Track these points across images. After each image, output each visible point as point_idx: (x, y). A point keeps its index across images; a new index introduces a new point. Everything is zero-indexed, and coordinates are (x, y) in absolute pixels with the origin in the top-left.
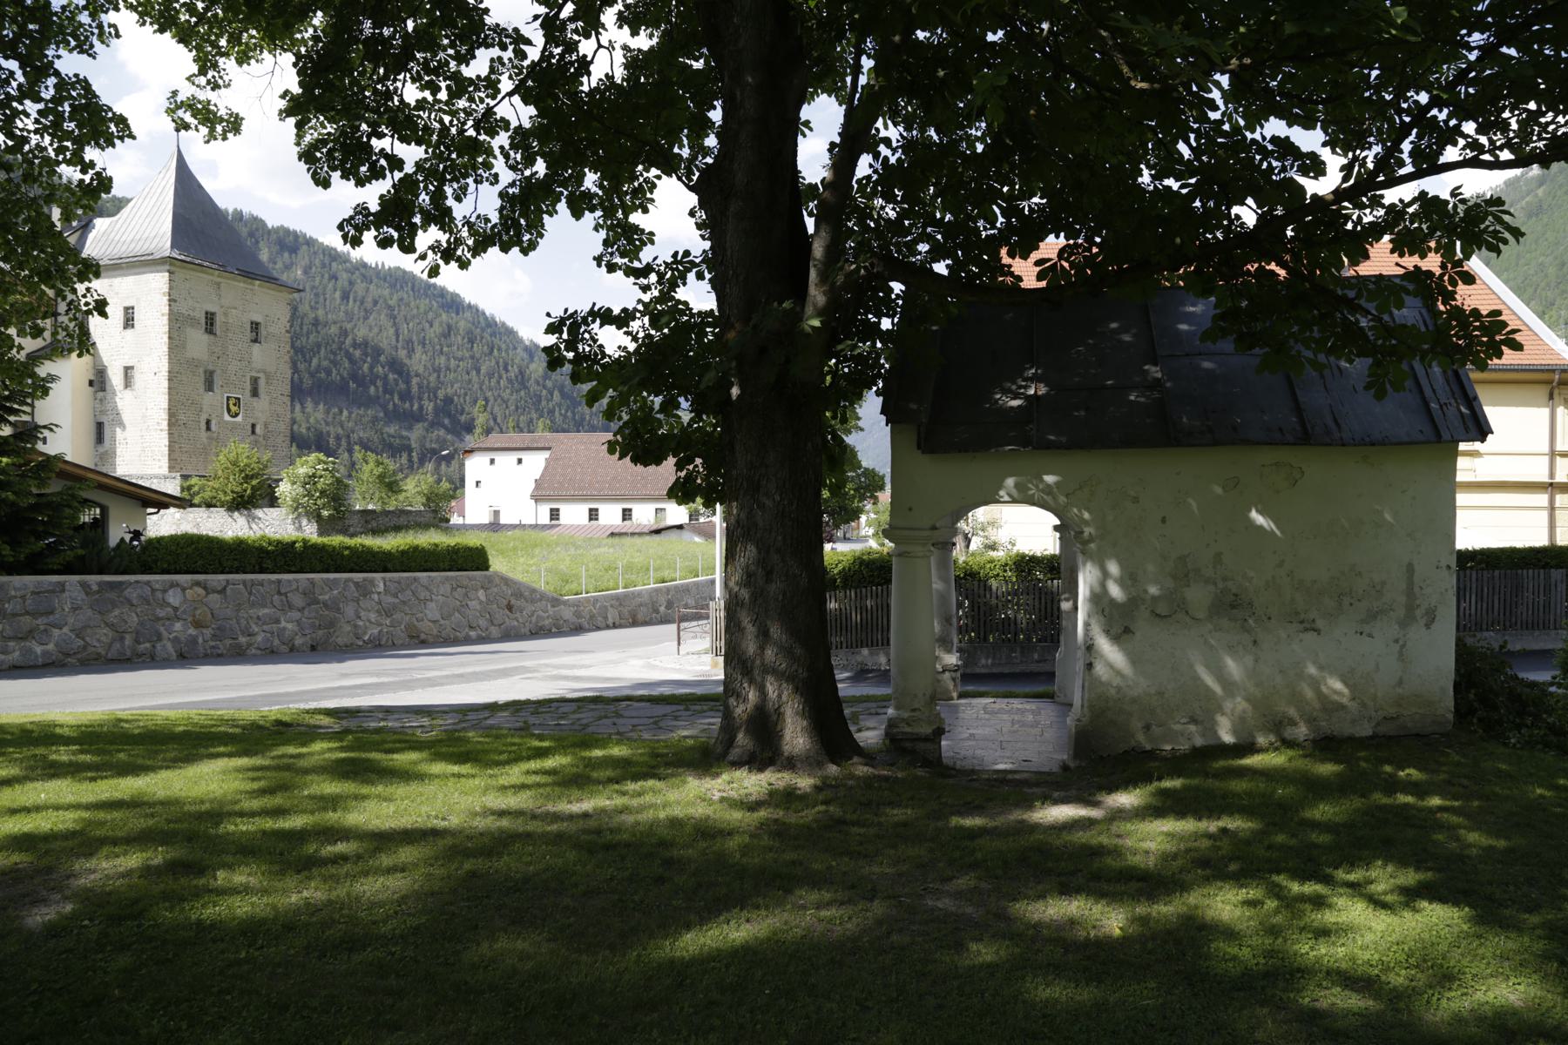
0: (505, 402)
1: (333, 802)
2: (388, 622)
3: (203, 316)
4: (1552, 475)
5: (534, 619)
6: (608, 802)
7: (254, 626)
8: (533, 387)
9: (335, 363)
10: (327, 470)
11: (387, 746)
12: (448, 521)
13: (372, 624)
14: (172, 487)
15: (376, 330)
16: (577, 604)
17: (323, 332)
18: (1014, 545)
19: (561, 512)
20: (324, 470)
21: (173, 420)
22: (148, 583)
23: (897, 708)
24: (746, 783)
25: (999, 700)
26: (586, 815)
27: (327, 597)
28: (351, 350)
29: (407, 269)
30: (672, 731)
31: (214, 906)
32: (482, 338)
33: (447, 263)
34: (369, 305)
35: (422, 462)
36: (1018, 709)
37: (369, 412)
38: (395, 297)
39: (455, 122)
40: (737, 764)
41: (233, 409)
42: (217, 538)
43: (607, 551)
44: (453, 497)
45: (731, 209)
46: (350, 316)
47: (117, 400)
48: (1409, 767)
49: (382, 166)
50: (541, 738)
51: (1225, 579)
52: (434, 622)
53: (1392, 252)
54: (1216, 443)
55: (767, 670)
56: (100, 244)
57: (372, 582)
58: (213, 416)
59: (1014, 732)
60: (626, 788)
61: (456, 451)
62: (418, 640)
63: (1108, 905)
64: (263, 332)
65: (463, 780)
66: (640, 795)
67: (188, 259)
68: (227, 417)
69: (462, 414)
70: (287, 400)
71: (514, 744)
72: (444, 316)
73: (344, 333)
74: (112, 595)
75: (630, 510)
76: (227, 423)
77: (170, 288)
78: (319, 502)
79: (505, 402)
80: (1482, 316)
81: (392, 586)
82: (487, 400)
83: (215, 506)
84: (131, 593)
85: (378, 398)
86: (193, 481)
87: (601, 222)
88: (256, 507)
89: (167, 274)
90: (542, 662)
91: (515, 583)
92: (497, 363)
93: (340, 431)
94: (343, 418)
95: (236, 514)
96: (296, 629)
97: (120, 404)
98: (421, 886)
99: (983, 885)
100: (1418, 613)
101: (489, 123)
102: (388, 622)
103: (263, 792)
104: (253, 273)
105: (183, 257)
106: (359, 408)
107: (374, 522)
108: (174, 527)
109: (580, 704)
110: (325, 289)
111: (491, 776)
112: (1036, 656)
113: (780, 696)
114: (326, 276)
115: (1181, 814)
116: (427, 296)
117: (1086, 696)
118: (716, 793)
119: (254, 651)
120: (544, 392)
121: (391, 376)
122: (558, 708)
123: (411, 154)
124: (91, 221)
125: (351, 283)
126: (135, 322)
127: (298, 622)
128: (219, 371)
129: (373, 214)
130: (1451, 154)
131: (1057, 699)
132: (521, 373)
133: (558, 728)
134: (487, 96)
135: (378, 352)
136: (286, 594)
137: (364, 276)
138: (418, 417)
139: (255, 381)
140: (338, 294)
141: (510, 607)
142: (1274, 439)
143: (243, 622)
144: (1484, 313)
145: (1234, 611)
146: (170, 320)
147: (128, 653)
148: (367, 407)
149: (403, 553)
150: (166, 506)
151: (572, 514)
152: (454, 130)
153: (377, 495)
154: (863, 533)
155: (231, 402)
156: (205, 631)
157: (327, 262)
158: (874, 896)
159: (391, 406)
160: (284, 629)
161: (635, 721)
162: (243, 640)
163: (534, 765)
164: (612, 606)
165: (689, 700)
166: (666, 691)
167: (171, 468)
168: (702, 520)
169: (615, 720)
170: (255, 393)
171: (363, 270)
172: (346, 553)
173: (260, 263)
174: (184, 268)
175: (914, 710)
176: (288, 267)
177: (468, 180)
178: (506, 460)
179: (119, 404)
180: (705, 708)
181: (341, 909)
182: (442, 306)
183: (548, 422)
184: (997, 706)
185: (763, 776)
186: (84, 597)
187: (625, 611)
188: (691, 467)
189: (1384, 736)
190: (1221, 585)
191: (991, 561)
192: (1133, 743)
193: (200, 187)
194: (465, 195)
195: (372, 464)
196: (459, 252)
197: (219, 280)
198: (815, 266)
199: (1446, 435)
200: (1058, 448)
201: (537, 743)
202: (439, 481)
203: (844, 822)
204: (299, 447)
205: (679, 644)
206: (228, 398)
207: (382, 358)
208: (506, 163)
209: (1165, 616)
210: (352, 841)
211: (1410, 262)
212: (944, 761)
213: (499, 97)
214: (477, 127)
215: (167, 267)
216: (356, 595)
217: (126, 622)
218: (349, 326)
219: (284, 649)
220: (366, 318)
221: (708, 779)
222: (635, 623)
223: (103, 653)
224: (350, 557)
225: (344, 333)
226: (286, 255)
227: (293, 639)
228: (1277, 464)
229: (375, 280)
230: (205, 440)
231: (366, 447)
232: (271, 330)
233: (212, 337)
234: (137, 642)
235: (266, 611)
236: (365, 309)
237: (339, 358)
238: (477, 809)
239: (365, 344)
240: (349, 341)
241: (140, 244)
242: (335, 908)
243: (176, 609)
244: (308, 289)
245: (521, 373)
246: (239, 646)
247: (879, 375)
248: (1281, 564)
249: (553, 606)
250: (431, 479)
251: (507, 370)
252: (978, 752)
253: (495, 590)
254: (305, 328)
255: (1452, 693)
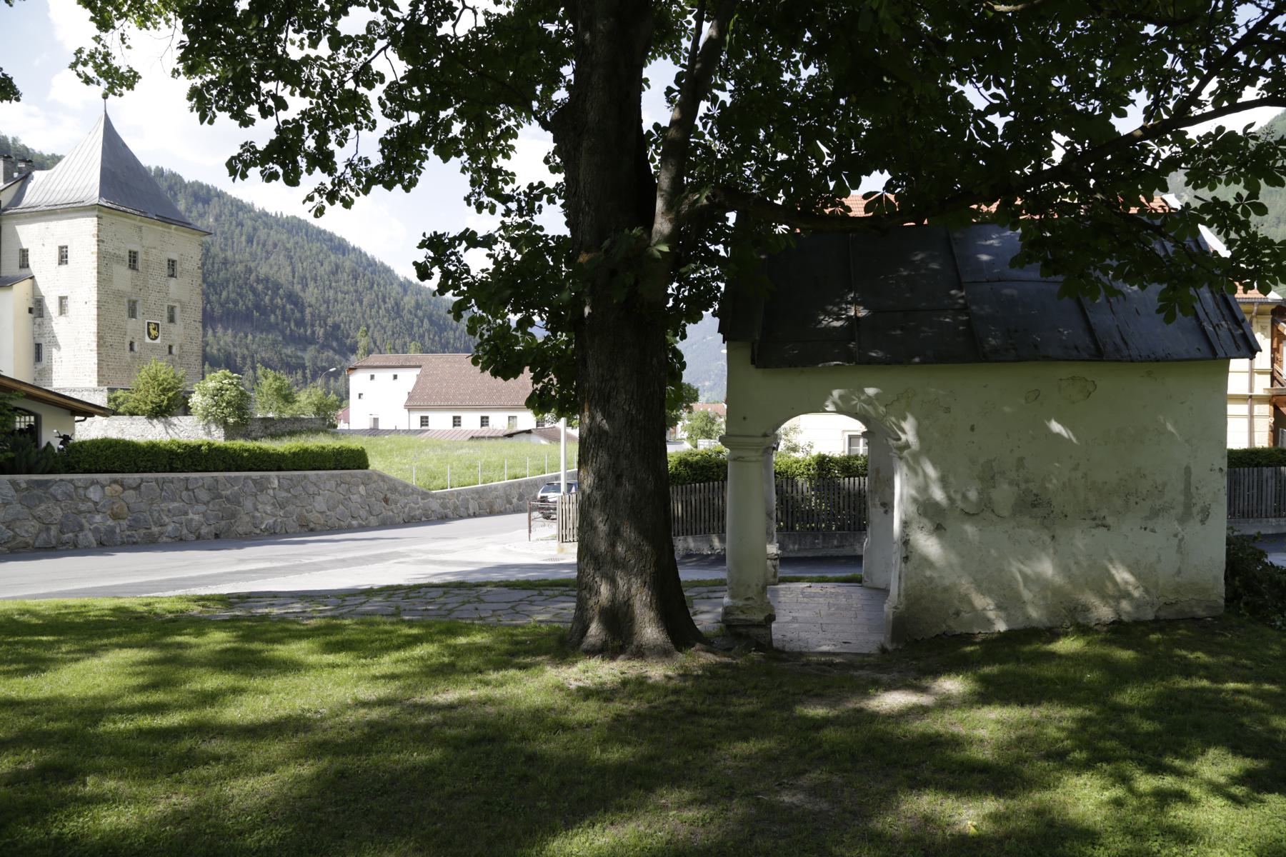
0: (384, 328)
1: (210, 698)
2: (281, 513)
3: (127, 254)
4: (1251, 389)
5: (407, 510)
6: (472, 693)
7: (165, 518)
8: (407, 316)
9: (241, 295)
10: (232, 384)
11: (269, 636)
12: (335, 426)
13: (267, 515)
14: (100, 399)
15: (276, 268)
16: (443, 497)
17: (231, 270)
18: (812, 447)
19: (430, 420)
20: (230, 384)
21: (101, 342)
22: (71, 481)
23: (732, 597)
24: (600, 673)
25: (813, 585)
26: (451, 707)
27: (229, 492)
28: (255, 284)
29: (302, 218)
30: (528, 616)
31: (79, 817)
32: (364, 275)
33: (332, 203)
34: (270, 248)
35: (314, 378)
36: (833, 593)
37: (270, 336)
38: (292, 241)
39: (336, 75)
40: (592, 652)
41: (153, 333)
42: (133, 442)
43: (468, 452)
44: (339, 407)
45: (585, 145)
46: (254, 256)
47: (53, 324)
48: (1200, 650)
49: (270, 107)
50: (411, 624)
51: (1027, 481)
52: (322, 513)
53: (1187, 184)
54: (1019, 359)
55: (618, 564)
56: (38, 194)
57: (268, 479)
58: (136, 339)
59: (831, 615)
60: (489, 678)
61: (342, 368)
62: (307, 529)
63: (957, 798)
64: (178, 268)
65: (337, 670)
66: (502, 685)
67: (114, 206)
68: (148, 340)
69: (347, 338)
70: (199, 326)
71: (386, 632)
72: (333, 257)
73: (249, 270)
74: (39, 492)
75: (487, 418)
76: (147, 344)
77: (99, 231)
78: (225, 411)
79: (384, 328)
80: (1275, 244)
81: (285, 483)
82: (368, 327)
83: (137, 415)
84: (57, 491)
85: (277, 324)
86: (119, 393)
87: (467, 165)
88: (172, 415)
89: (96, 219)
90: (413, 547)
91: (391, 479)
92: (377, 296)
93: (246, 352)
94: (248, 341)
95: (155, 421)
96: (202, 519)
97: (56, 328)
98: (290, 789)
99: (836, 779)
100: (1195, 510)
101: (366, 76)
102: (281, 513)
103: (142, 689)
104: (170, 219)
105: (109, 205)
106: (261, 333)
107: (273, 428)
108: (102, 432)
109: (445, 589)
110: (233, 233)
111: (363, 666)
112: (835, 542)
113: (629, 590)
114: (234, 223)
115: (1005, 701)
116: (318, 240)
117: (903, 585)
118: (573, 682)
119: (165, 539)
120: (416, 320)
121: (288, 307)
122: (426, 593)
123: (297, 105)
124: (30, 173)
125: (255, 229)
126: (69, 259)
127: (204, 514)
128: (140, 302)
129: (259, 152)
130: (1249, 94)
131: (864, 583)
132: (397, 304)
133: (425, 613)
134: (364, 52)
135: (277, 286)
136: (193, 490)
137: (265, 223)
138: (310, 341)
139: (172, 309)
140: (243, 238)
141: (386, 500)
142: (1070, 355)
143: (156, 514)
144: (1277, 241)
145: (1035, 509)
146: (98, 257)
147: (54, 542)
148: (268, 332)
149: (295, 454)
150: (91, 415)
151: (440, 421)
152: (335, 82)
153: (275, 405)
154: (679, 436)
155: (151, 327)
156: (121, 522)
157: (234, 211)
158: (732, 793)
159: (288, 332)
160: (192, 520)
161: (495, 606)
162: (155, 529)
163: (402, 654)
164: (472, 498)
165: (542, 586)
166: (521, 576)
167: (100, 383)
168: (547, 426)
169: (477, 605)
170: (172, 320)
171: (265, 219)
172: (246, 454)
173: (179, 213)
174: (110, 213)
175: (747, 599)
176: (201, 216)
177: (348, 127)
178: (384, 376)
179: (55, 328)
180: (557, 593)
181: (209, 817)
182: (331, 249)
183: (419, 344)
184: (813, 590)
185: (615, 664)
186: (14, 493)
187: (484, 502)
188: (546, 380)
189: (1165, 620)
190: (1023, 486)
191: (797, 462)
192: (944, 628)
193: (124, 145)
194: (346, 140)
195: (271, 379)
196: (343, 193)
197: (141, 224)
198: (662, 196)
199: (1221, 353)
200: (879, 363)
201: (407, 631)
202: (327, 394)
203: (696, 713)
204: (211, 365)
205: (530, 531)
206: (149, 323)
207: (281, 292)
208: (383, 112)
209: (973, 514)
210: (226, 738)
211: (1206, 194)
212: (775, 644)
213: (374, 53)
214: (356, 78)
215: (96, 213)
216: (254, 490)
217: (52, 515)
218: (253, 265)
219: (192, 537)
220: (267, 258)
221: (564, 667)
222: (492, 513)
223: (31, 542)
224: (248, 459)
225: (249, 271)
226: (200, 205)
227: (199, 528)
228: (1073, 378)
229: (275, 227)
230: (129, 359)
231: (267, 365)
232: (186, 266)
233: (135, 272)
234: (62, 532)
235: (176, 504)
236: (267, 251)
237: (244, 291)
238: (349, 701)
239: (267, 279)
240: (253, 277)
241: (74, 192)
242: (202, 816)
243: (96, 503)
244: (218, 234)
245: (397, 304)
246: (152, 535)
247: (715, 298)
248: (1076, 468)
249: (423, 499)
250: (320, 392)
251: (385, 302)
252: (803, 635)
253: (374, 485)
254: (216, 266)
255: (1223, 581)
